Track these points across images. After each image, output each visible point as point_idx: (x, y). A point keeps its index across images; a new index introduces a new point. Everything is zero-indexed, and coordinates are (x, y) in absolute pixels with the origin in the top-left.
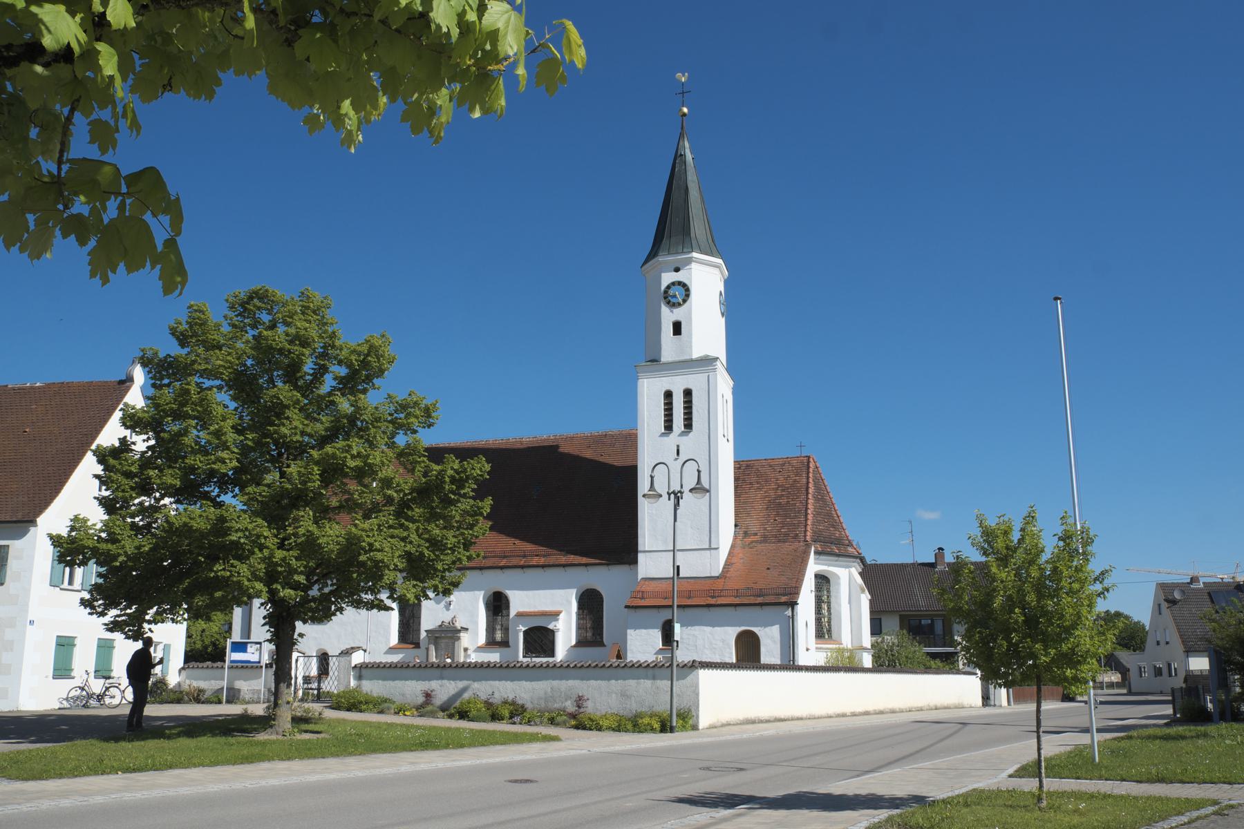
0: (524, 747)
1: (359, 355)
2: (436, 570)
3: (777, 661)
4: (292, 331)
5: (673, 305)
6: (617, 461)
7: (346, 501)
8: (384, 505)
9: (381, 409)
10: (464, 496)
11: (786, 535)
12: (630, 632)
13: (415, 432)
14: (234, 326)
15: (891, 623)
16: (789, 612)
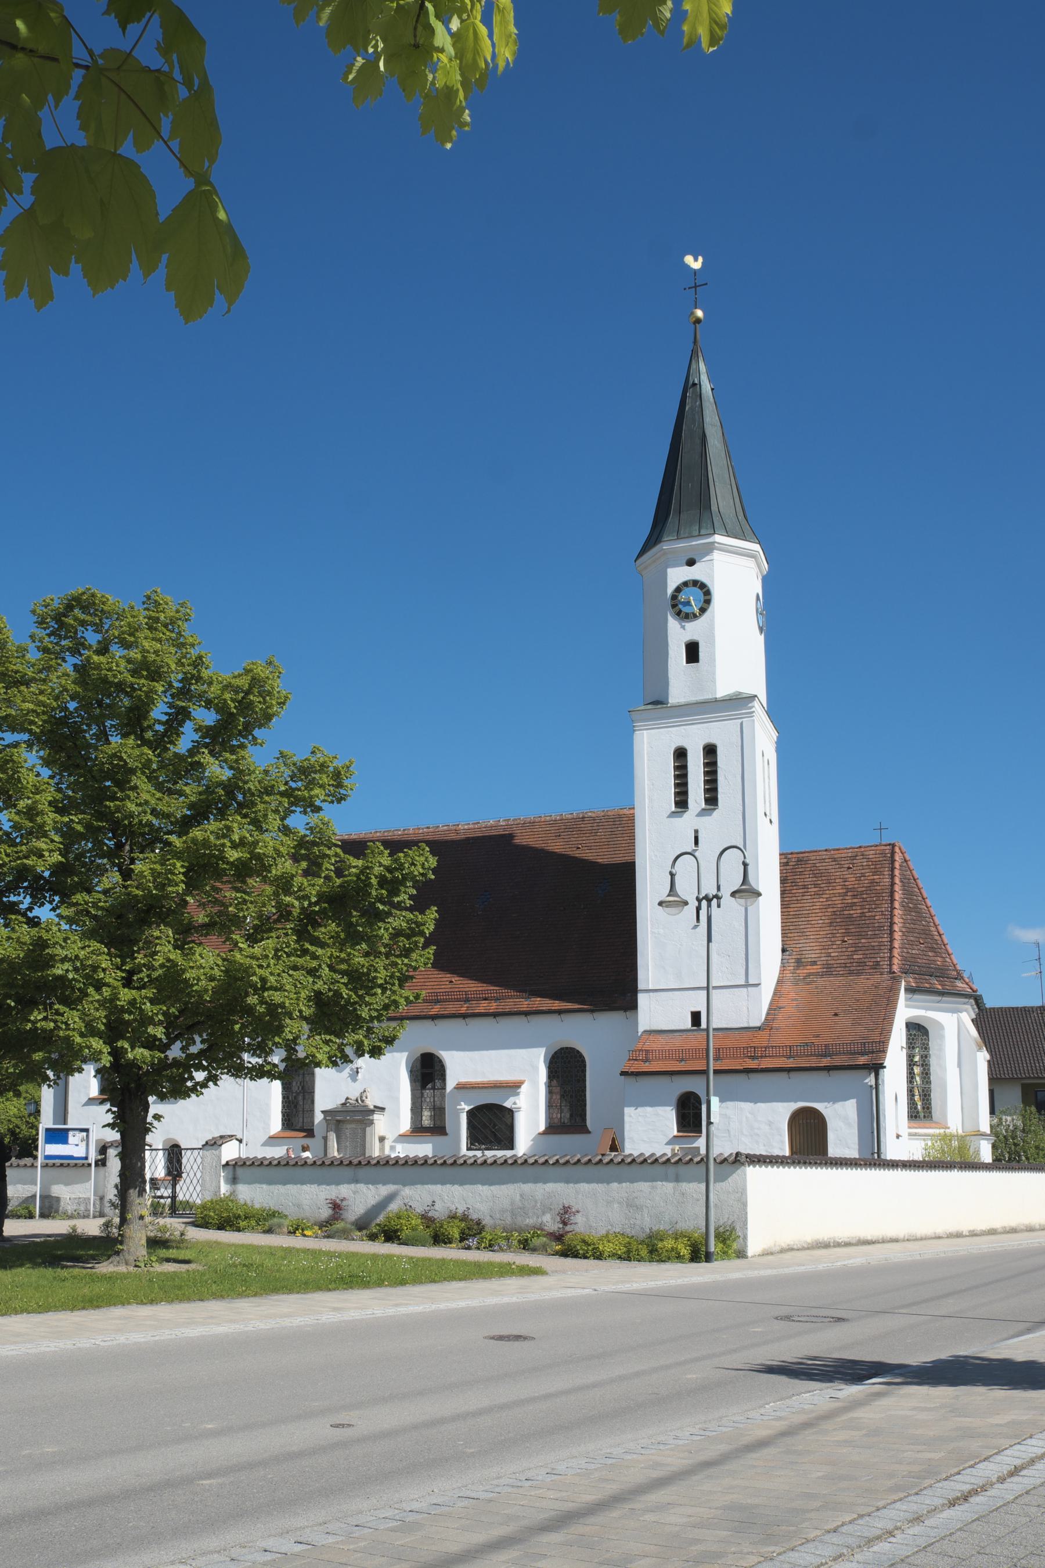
0: (495, 1284)
1: (237, 692)
2: (359, 1018)
3: (853, 1153)
4: (135, 654)
5: (685, 617)
6: (603, 857)
7: (220, 914)
8: (276, 921)
9: (273, 771)
10: (398, 906)
11: (861, 963)
12: (628, 1111)
13: (318, 809)
14: (45, 650)
15: (1013, 1095)
16: (871, 1080)
